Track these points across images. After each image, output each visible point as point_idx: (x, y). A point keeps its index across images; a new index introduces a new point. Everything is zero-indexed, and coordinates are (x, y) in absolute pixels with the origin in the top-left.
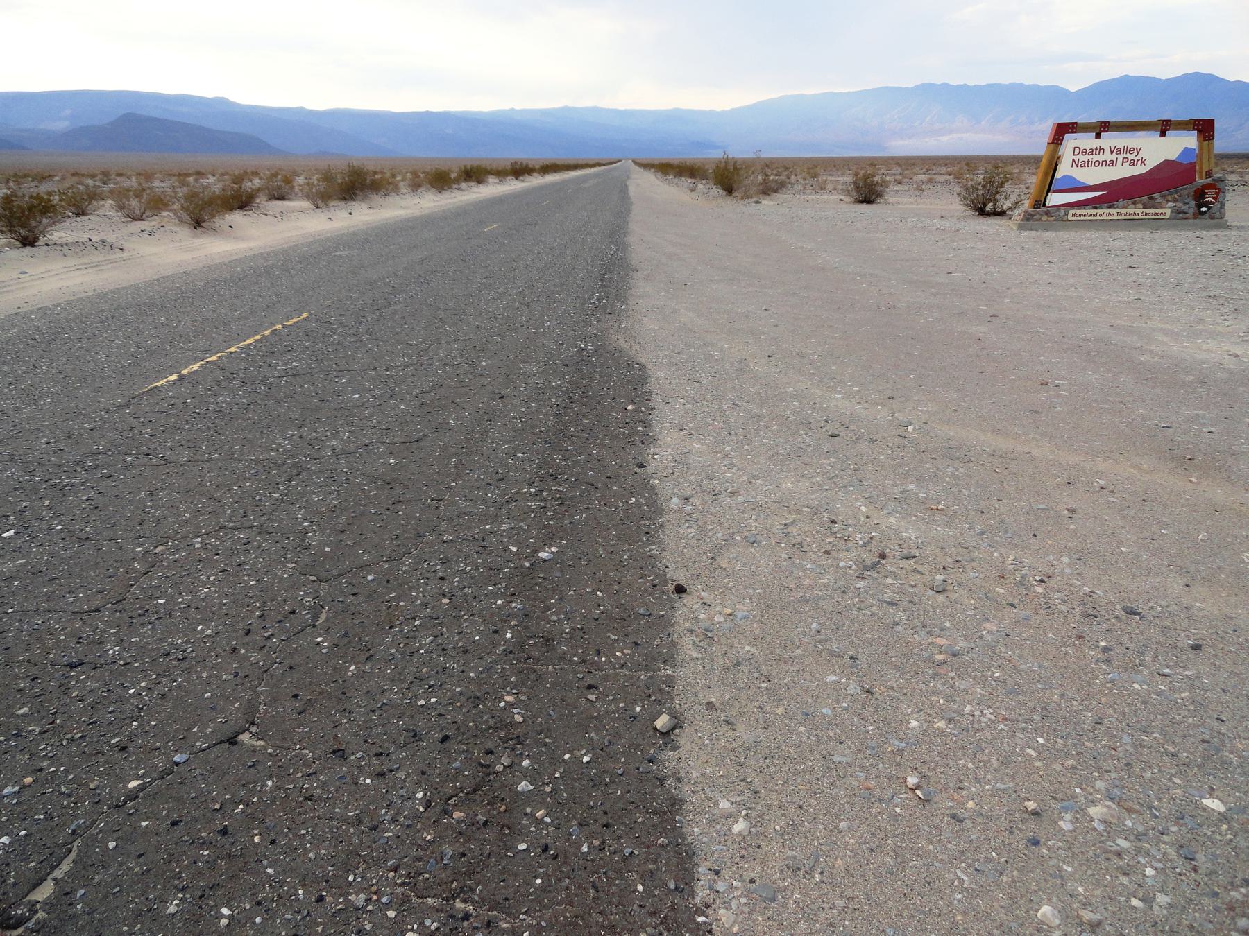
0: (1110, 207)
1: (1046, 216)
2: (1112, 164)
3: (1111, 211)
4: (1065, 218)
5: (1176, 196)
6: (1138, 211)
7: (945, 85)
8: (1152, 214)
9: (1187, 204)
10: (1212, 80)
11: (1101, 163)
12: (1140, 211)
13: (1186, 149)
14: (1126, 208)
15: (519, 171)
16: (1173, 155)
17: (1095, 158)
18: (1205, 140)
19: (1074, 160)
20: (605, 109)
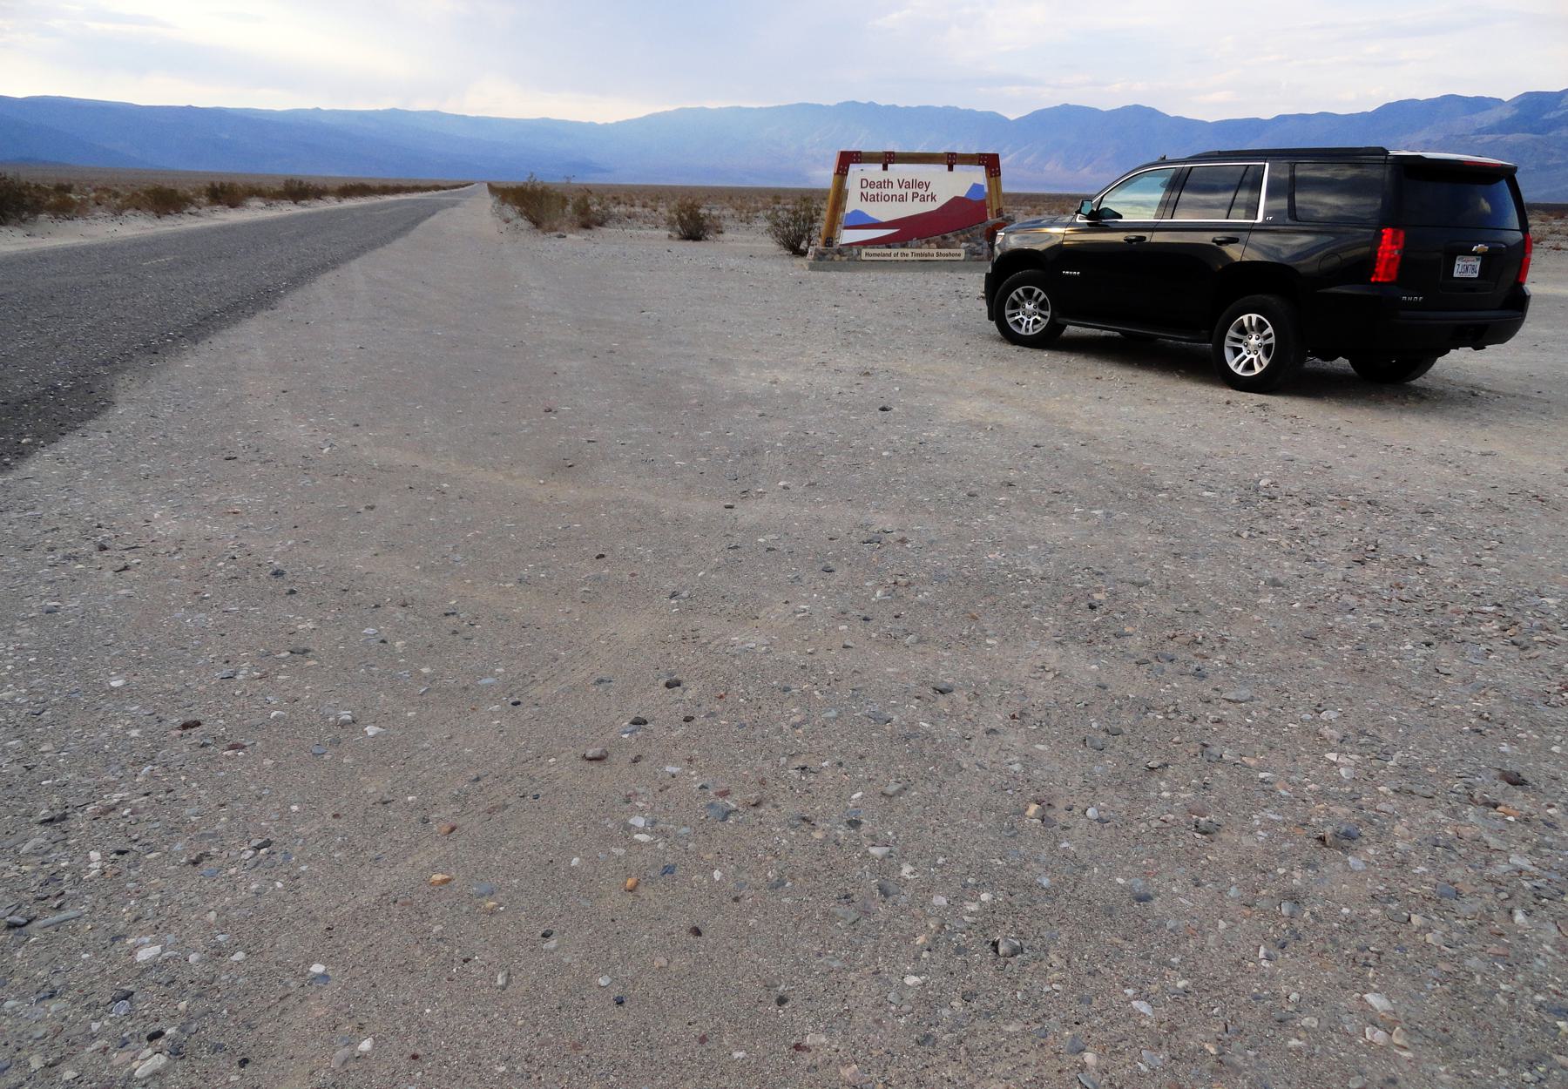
0: (904, 246)
1: (838, 256)
2: (902, 199)
3: (906, 251)
4: (858, 258)
5: (968, 236)
6: (933, 252)
7: (872, 105)
8: (947, 255)
9: (980, 244)
10: (1152, 113)
12: (934, 251)
14: (920, 248)
15: (298, 192)
16: (962, 192)
17: (885, 191)
18: (992, 176)
19: (862, 193)
20: (635, 120)
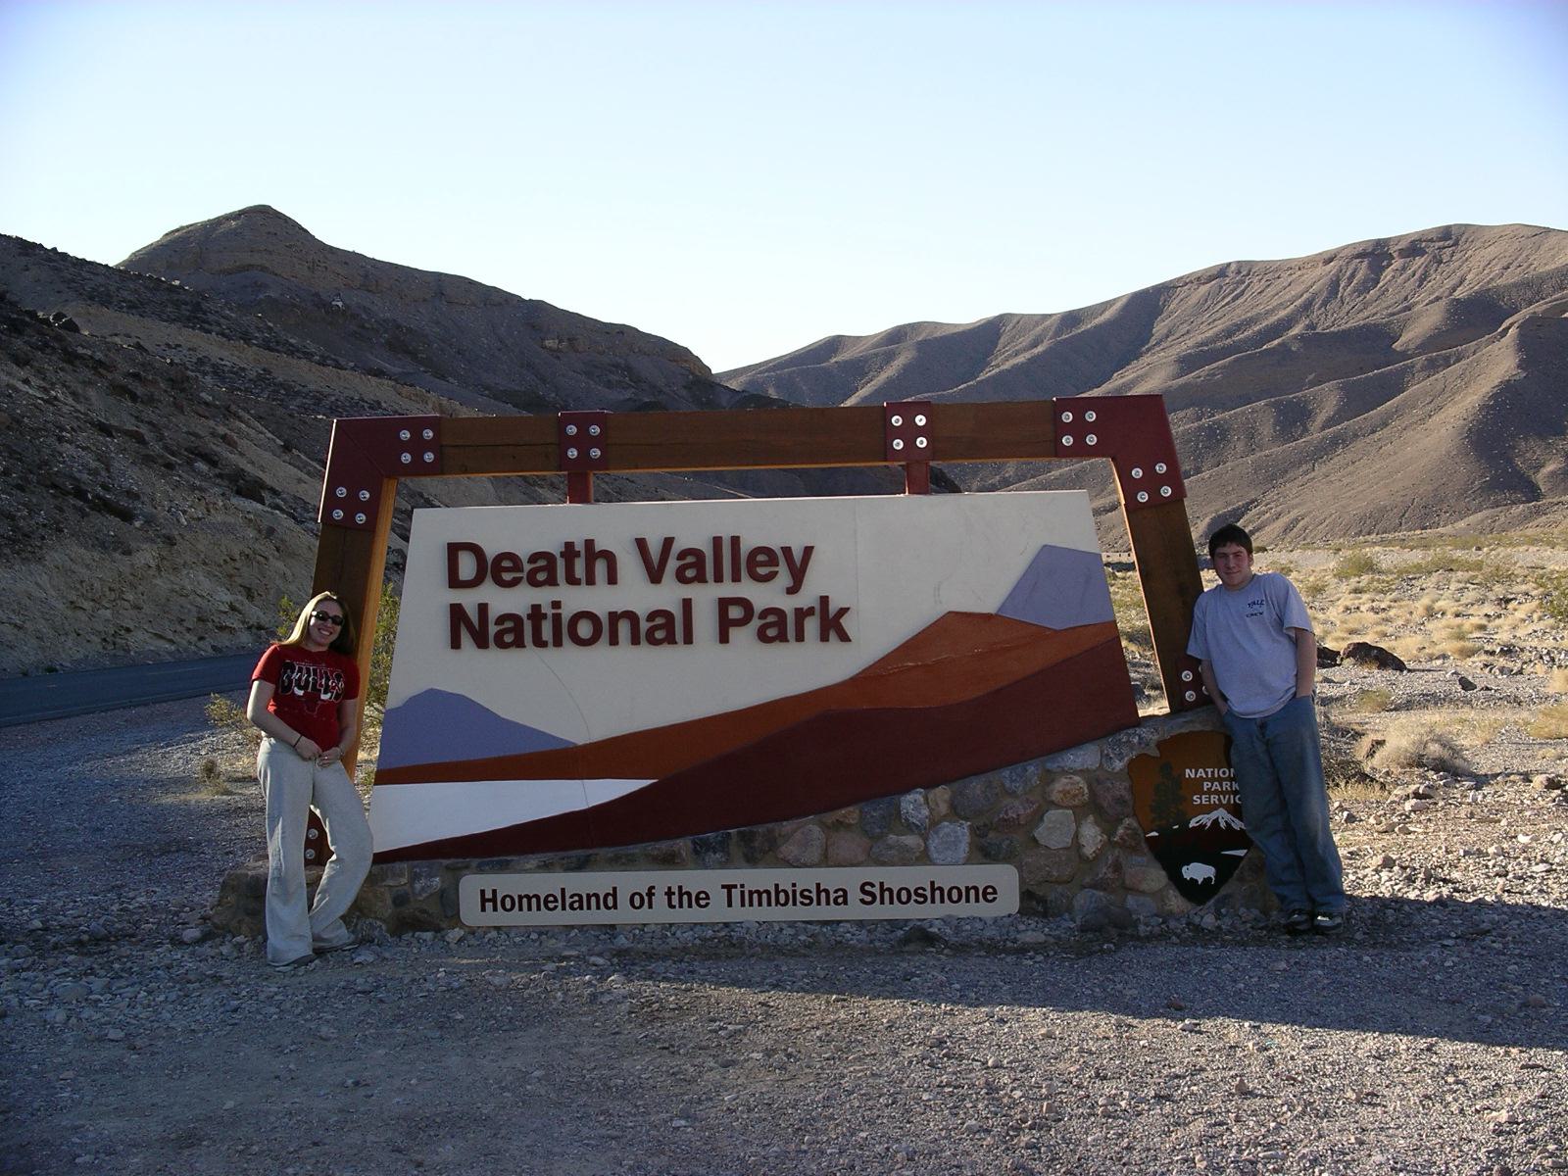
11: (607, 629)
12: (850, 878)
13: (1047, 550)
17: (574, 599)
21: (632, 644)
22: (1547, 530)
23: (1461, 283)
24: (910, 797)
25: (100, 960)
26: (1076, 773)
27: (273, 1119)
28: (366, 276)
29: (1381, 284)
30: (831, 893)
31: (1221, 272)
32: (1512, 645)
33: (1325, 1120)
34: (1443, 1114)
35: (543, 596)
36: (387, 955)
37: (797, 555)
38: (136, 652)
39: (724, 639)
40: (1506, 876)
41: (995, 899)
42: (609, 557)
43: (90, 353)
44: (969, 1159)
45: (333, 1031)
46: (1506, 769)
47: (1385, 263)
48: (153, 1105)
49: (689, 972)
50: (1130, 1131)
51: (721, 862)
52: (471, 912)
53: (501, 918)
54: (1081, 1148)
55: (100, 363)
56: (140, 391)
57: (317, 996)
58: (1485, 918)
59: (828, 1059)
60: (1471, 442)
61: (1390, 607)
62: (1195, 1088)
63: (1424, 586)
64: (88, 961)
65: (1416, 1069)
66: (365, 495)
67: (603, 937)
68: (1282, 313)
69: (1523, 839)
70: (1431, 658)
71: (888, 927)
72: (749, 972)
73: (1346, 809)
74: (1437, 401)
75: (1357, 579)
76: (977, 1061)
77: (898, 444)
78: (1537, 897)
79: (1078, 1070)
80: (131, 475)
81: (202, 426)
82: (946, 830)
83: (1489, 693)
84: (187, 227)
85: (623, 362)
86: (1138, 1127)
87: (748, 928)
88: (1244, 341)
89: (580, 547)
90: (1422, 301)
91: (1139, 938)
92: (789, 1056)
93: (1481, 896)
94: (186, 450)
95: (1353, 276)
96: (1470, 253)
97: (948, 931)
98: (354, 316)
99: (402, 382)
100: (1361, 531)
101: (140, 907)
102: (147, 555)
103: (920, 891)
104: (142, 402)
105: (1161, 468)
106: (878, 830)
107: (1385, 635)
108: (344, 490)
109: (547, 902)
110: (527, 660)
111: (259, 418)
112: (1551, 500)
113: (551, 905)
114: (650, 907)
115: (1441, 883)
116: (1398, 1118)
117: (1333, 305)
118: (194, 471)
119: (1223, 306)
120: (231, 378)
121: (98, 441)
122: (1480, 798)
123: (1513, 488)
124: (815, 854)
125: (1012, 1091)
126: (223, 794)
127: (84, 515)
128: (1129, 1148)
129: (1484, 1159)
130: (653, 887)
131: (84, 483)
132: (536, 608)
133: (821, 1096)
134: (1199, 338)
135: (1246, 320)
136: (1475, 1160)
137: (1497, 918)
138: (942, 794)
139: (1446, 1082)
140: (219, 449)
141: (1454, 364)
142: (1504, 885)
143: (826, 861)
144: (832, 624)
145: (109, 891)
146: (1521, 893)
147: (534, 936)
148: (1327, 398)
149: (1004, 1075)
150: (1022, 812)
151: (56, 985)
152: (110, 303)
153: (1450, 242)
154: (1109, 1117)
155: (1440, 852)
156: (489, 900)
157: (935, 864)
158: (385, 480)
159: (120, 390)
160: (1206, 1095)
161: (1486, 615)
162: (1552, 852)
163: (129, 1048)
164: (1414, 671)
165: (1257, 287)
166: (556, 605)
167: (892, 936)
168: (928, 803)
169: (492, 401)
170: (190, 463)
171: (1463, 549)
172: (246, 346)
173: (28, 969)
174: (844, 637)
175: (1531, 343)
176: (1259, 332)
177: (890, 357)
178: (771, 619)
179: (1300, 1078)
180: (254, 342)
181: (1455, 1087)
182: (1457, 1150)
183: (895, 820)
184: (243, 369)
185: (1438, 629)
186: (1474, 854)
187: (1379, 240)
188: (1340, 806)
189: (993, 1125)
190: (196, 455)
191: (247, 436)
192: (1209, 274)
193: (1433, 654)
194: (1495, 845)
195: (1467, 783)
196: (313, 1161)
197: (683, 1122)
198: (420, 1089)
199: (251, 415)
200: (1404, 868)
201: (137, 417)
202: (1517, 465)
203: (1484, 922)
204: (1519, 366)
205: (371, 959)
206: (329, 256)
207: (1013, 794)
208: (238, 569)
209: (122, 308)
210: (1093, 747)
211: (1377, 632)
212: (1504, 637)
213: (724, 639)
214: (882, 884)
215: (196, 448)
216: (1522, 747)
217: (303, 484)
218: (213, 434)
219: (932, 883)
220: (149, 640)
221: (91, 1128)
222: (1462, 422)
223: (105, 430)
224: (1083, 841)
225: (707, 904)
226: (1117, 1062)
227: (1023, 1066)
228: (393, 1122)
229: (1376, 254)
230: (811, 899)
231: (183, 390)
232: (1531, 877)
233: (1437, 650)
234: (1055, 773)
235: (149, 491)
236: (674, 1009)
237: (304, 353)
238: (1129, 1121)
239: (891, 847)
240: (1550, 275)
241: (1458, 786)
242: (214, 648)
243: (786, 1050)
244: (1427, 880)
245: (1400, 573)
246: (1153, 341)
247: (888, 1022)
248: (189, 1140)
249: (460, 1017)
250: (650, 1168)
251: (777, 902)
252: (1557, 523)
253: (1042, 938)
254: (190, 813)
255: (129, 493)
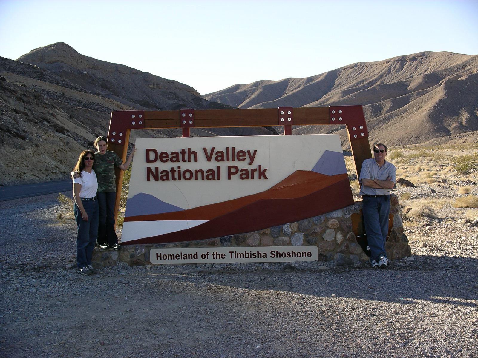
12: (267, 250)
13: (327, 153)
17: (184, 166)
21: (202, 180)
22: (453, 144)
23: (428, 69)
24: (286, 226)
25: (42, 274)
26: (335, 218)
27: (107, 321)
28: (94, 64)
29: (404, 69)
30: (262, 254)
31: (356, 65)
32: (445, 179)
33: (422, 321)
34: (456, 319)
35: (175, 165)
36: (129, 273)
37: (252, 153)
38: (27, 180)
39: (230, 178)
40: (460, 249)
41: (311, 256)
42: (195, 153)
43: (9, 87)
44: (319, 333)
45: (118, 295)
46: (447, 217)
47: (405, 63)
48: (70, 317)
49: (222, 278)
50: (365, 324)
51: (229, 245)
52: (153, 259)
53: (163, 262)
54: (351, 329)
55: (13, 91)
56: (25, 99)
57: (111, 285)
58: (457, 261)
59: (271, 304)
60: (430, 118)
61: (407, 168)
62: (382, 312)
63: (417, 161)
64: (39, 274)
65: (445, 306)
66: (121, 134)
67: (193, 267)
68: (374, 78)
69: (463, 238)
70: (422, 183)
71: (279, 264)
72: (241, 278)
73: (409, 229)
74: (420, 105)
75: (397, 159)
76: (315, 304)
77: (282, 120)
78: (471, 255)
79: (346, 307)
80: (24, 126)
81: (45, 111)
82: (296, 236)
83: (440, 194)
84: (38, 48)
85: (173, 92)
86: (367, 323)
87: (237, 265)
88: (362, 87)
89: (186, 150)
90: (416, 75)
91: (354, 268)
92: (259, 302)
93: (454, 255)
94: (40, 118)
95: (395, 67)
96: (430, 60)
97: (297, 265)
98: (90, 77)
99: (106, 97)
100: (397, 145)
101: (49, 258)
102: (30, 150)
103: (289, 254)
104: (26, 103)
105: (361, 127)
106: (276, 236)
107: (407, 176)
108: (115, 133)
109: (176, 257)
110: (170, 184)
111: (62, 108)
112: (454, 135)
113: (178, 258)
114: (208, 258)
115: (441, 251)
116: (443, 320)
117: (389, 75)
118: (43, 124)
119: (356, 76)
120: (53, 96)
121: (14, 115)
122: (446, 226)
123: (443, 132)
124: (257, 242)
125: (327, 313)
126: (65, 224)
127: (10, 138)
128: (366, 330)
129: (471, 332)
130: (208, 252)
131: (10, 128)
132: (173, 169)
133: (271, 314)
134: (349, 86)
135: (363, 80)
136: (469, 332)
137: (461, 262)
138: (295, 225)
139: (455, 310)
140: (50, 118)
141: (425, 94)
142: (461, 252)
143: (260, 245)
144: (262, 174)
145: (38, 253)
146: (466, 254)
147: (173, 267)
148: (387, 104)
149: (324, 308)
150: (319, 230)
151: (30, 281)
152: (15, 72)
153: (425, 57)
154: (358, 320)
155: (439, 242)
156: (159, 256)
157: (293, 246)
158: (127, 130)
159: (20, 99)
160: (385, 314)
161: (437, 170)
162: (473, 242)
163: (57, 300)
164: (417, 187)
165: (366, 70)
166: (179, 168)
167: (280, 267)
168: (291, 228)
169: (133, 103)
170: (41, 122)
171: (428, 150)
172: (57, 86)
173: (20, 276)
174: (266, 178)
175: (448, 87)
176: (367, 84)
177: (254, 91)
178: (244, 172)
179: (412, 309)
180: (60, 84)
181: (458, 311)
182: (463, 330)
183: (281, 233)
184: (56, 93)
185: (423, 174)
186: (450, 243)
187: (403, 56)
188: (407, 228)
189: (324, 323)
190: (43, 119)
191: (59, 114)
192: (352, 66)
193: (422, 182)
194: (455, 240)
195: (436, 221)
196: (123, 333)
197: (231, 322)
198: (150, 312)
199: (59, 107)
200: (430, 247)
201: (25, 108)
202: (444, 125)
203: (457, 263)
204: (445, 95)
205: (125, 274)
206: (82, 58)
207: (317, 225)
208: (58, 155)
209: (18, 73)
210: (340, 211)
211: (404, 175)
212: (443, 177)
213: (230, 178)
214: (277, 252)
215: (43, 117)
216: (451, 210)
217: (76, 129)
218: (48, 113)
219: (292, 251)
220: (31, 176)
221: (53, 323)
222: (427, 111)
223: (16, 112)
224: (337, 239)
225: (225, 257)
226: (357, 304)
227: (329, 305)
228: (144, 322)
229: (402, 60)
230: (256, 256)
231: (39, 99)
232: (468, 249)
233: (423, 181)
234: (330, 218)
235: (30, 130)
236: (221, 289)
237: (75, 88)
238: (364, 321)
239: (280, 241)
240: (454, 67)
241: (434, 222)
242: (51, 179)
243: (257, 301)
244: (437, 250)
245: (410, 157)
246: (335, 86)
247: (286, 293)
248: (83, 327)
249: (156, 291)
250: (224, 335)
251: (246, 257)
252: (456, 142)
253: (326, 268)
254: (57, 230)
255: (24, 131)
